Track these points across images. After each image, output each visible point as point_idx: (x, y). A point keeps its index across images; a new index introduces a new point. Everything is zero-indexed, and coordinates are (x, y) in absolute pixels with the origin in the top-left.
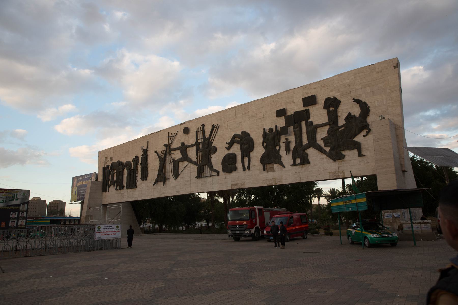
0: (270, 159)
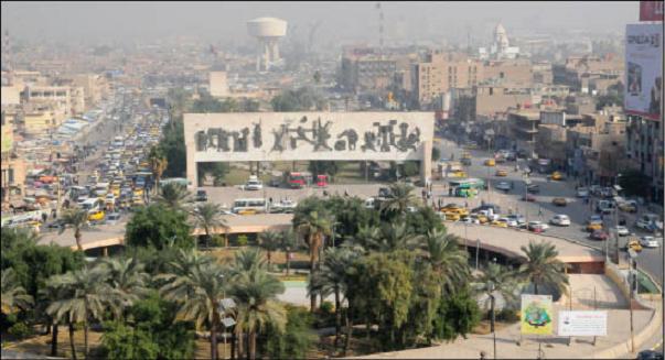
0: (368, 145)
